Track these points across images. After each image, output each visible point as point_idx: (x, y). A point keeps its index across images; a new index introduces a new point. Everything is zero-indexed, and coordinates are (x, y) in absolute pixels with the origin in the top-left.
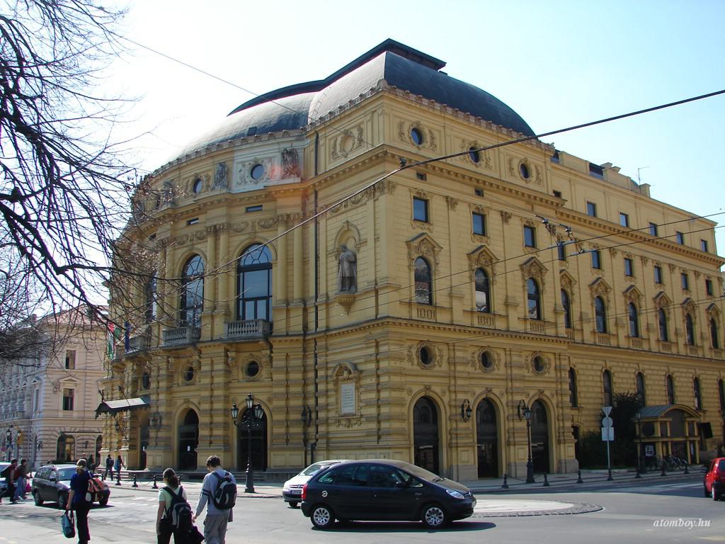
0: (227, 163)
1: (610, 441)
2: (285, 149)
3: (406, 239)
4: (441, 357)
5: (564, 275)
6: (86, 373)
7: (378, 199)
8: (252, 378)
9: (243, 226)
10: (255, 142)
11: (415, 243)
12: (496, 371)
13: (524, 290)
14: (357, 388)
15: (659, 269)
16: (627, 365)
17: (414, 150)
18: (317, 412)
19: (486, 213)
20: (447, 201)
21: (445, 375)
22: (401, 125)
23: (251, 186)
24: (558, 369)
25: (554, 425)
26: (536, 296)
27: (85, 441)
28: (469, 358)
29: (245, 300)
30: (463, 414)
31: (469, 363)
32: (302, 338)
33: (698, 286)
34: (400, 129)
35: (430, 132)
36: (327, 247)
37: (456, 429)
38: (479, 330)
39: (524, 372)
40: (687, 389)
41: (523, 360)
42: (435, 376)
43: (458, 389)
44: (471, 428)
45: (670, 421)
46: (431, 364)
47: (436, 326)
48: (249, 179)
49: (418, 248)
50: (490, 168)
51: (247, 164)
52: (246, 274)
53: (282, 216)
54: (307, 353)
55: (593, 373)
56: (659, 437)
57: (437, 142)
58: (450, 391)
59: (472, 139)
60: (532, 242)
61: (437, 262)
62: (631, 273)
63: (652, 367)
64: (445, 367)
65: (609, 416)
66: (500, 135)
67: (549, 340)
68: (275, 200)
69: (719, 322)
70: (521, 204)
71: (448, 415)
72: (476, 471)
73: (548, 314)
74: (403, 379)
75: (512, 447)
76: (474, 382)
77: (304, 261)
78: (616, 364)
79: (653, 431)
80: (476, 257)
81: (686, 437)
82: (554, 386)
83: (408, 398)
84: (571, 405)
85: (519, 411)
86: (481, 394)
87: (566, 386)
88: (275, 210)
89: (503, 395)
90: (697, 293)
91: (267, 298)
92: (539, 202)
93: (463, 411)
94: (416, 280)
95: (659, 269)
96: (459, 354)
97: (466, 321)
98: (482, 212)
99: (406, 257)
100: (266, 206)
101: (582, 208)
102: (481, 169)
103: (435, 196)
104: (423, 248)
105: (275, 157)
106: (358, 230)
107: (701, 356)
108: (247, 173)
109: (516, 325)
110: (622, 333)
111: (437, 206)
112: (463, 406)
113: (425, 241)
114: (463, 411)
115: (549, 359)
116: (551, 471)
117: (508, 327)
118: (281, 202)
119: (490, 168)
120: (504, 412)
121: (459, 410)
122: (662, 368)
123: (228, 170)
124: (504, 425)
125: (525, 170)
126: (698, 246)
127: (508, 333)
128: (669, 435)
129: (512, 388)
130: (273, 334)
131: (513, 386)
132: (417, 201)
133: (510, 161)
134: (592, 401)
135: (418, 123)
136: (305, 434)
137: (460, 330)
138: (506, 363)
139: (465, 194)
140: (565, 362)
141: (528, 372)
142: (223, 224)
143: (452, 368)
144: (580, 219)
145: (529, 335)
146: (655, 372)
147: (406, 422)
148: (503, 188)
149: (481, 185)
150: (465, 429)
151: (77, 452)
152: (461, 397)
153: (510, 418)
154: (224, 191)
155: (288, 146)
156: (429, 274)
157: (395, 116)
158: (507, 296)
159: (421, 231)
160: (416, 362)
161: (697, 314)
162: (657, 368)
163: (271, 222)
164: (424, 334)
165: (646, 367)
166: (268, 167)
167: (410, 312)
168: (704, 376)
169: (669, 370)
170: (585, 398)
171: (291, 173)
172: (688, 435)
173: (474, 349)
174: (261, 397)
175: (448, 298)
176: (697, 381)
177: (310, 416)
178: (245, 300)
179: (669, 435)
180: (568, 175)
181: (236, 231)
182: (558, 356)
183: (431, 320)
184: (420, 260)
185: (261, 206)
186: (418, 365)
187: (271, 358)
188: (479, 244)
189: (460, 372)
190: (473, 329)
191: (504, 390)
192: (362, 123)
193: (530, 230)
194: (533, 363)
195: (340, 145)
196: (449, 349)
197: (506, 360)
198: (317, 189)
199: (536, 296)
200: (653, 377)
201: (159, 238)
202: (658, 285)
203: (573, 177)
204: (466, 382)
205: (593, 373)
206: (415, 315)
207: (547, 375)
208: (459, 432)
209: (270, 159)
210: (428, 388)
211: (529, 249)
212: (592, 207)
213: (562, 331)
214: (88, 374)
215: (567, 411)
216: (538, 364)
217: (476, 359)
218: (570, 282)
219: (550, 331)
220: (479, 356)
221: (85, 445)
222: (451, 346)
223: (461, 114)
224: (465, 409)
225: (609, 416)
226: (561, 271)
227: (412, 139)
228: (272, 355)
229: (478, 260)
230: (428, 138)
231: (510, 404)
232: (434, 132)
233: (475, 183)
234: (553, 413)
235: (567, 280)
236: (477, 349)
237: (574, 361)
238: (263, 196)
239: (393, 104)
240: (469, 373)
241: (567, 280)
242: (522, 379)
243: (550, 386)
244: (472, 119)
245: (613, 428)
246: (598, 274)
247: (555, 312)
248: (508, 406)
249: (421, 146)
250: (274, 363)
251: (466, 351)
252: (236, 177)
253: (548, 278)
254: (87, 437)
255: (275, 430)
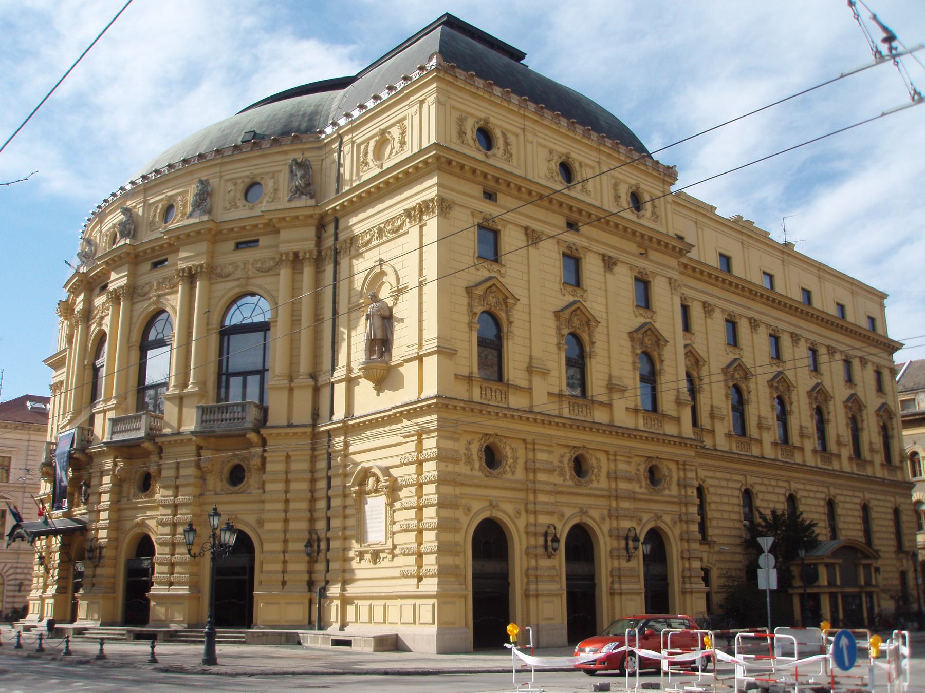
0: (211, 181)
1: (772, 591)
2: (295, 160)
3: (465, 284)
4: (515, 460)
5: (691, 354)
6: (24, 488)
7: (425, 225)
8: (233, 489)
9: (230, 268)
10: (252, 150)
11: (479, 291)
12: (595, 485)
13: (634, 369)
14: (390, 505)
15: (814, 351)
16: (774, 483)
17: (480, 156)
18: (328, 540)
19: (582, 256)
20: (526, 234)
21: (519, 486)
22: (461, 121)
23: (242, 212)
24: (682, 484)
25: (675, 566)
26: (650, 378)
27: (18, 582)
28: (556, 462)
29: (230, 375)
30: (546, 546)
31: (554, 471)
32: (309, 430)
33: (865, 378)
34: (461, 126)
35: (504, 134)
36: (350, 298)
37: (536, 568)
38: (570, 422)
39: (636, 487)
40: (853, 520)
41: (632, 469)
42: (506, 488)
43: (539, 507)
44: (557, 567)
45: (839, 564)
46: (500, 469)
47: (509, 413)
48: (241, 202)
49: (483, 298)
50: (588, 193)
51: (239, 181)
52: (232, 337)
53: (287, 254)
54: (317, 453)
55: (729, 492)
56: (825, 587)
57: (513, 149)
58: (527, 511)
59: (564, 151)
60: (645, 301)
61: (511, 319)
62: (777, 356)
63: (808, 487)
64: (520, 474)
65: (769, 552)
66: (602, 148)
67: (664, 441)
68: (277, 232)
69: (893, 429)
70: (633, 247)
71: (524, 547)
72: (565, 632)
73: (667, 403)
74: (458, 491)
75: (617, 598)
76: (564, 499)
77: (317, 318)
78: (759, 480)
79: (815, 577)
80: (567, 316)
81: (860, 586)
82: (675, 508)
83: (465, 520)
84: (699, 536)
85: (627, 544)
86: (572, 516)
87: (694, 510)
88: (277, 246)
89: (604, 519)
90: (864, 388)
91: (261, 372)
92: (655, 246)
93: (546, 541)
94: (479, 345)
95: (814, 351)
96: (541, 456)
97: (552, 408)
98: (576, 254)
99: (465, 309)
100: (263, 241)
101: (713, 261)
102: (576, 193)
103: (509, 226)
104: (491, 298)
105: (280, 171)
106: (396, 271)
107: (870, 474)
108: (240, 195)
109: (623, 418)
110: (768, 438)
111: (511, 239)
112: (546, 535)
113: (494, 289)
114: (546, 541)
115: (671, 472)
116: (598, 631)
117: (612, 420)
118: (284, 235)
119: (588, 193)
120: (605, 545)
121: (541, 541)
122: (821, 489)
123: (212, 191)
124: (605, 564)
125: (636, 201)
126: (864, 324)
127: (612, 429)
128: (838, 583)
129: (617, 510)
130: (268, 424)
131: (613, 511)
132: (483, 231)
133: (616, 186)
134: (727, 532)
135: (487, 121)
136: (310, 572)
137: (543, 421)
138: (608, 473)
139: (550, 222)
140: (691, 475)
141: (641, 487)
142: (201, 266)
143: (531, 476)
144: (710, 275)
145: (641, 434)
146: (812, 494)
147: (462, 555)
148: (603, 220)
149: (575, 216)
150: (549, 568)
151: (8, 597)
152: (544, 520)
153: (615, 553)
154: (206, 218)
155: (299, 157)
156: (499, 337)
157: (453, 108)
158: (610, 376)
159: (487, 274)
160: (477, 465)
161: (865, 417)
162: (815, 488)
163: (271, 263)
164: (492, 425)
165: (800, 486)
166: (269, 184)
167: (470, 390)
168: (876, 503)
169: (829, 491)
170: (718, 527)
171: (302, 193)
172: (863, 583)
173: (562, 451)
174: (247, 522)
175: (526, 374)
176: (865, 508)
177: (319, 546)
178: (230, 375)
179: (838, 583)
180: (693, 215)
181: (220, 276)
182: (682, 465)
183: (500, 405)
184: (485, 315)
185: (257, 241)
186: (480, 469)
187: (264, 460)
188: (571, 299)
189: (540, 482)
190: (563, 421)
191: (606, 512)
192: (404, 118)
193: (643, 284)
194: (647, 474)
195: (374, 151)
196: (526, 448)
197: (609, 468)
198: (338, 215)
199: (650, 378)
200: (809, 501)
201: (111, 287)
202: (814, 374)
203: (700, 218)
204: (552, 499)
205: (729, 492)
206: (476, 395)
207: (666, 492)
208: (539, 573)
209: (273, 175)
210: (492, 506)
211: (641, 311)
212: (726, 260)
213: (687, 429)
214: (27, 490)
215: (695, 546)
216: (654, 476)
217: (566, 465)
218: (697, 362)
219: (670, 429)
220: (570, 460)
221: (17, 588)
222: (530, 445)
223: (548, 113)
224: (549, 539)
225: (769, 552)
226: (686, 346)
227: (477, 142)
228: (265, 454)
229: (569, 321)
230: (500, 142)
231: (615, 533)
232: (509, 135)
233: (566, 211)
234: (675, 549)
235: (694, 359)
236: (567, 450)
237: (702, 474)
238: (261, 226)
239: (449, 89)
240: (555, 485)
241: (694, 359)
242: (632, 497)
243: (667, 511)
244: (564, 122)
245: (775, 570)
246: (735, 354)
247: (679, 403)
248: (611, 536)
249: (489, 153)
250: (269, 467)
251: (551, 452)
252: (219, 203)
253: (667, 352)
254: (22, 576)
255: (266, 567)
